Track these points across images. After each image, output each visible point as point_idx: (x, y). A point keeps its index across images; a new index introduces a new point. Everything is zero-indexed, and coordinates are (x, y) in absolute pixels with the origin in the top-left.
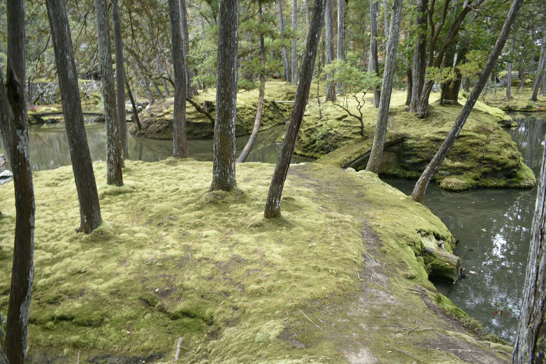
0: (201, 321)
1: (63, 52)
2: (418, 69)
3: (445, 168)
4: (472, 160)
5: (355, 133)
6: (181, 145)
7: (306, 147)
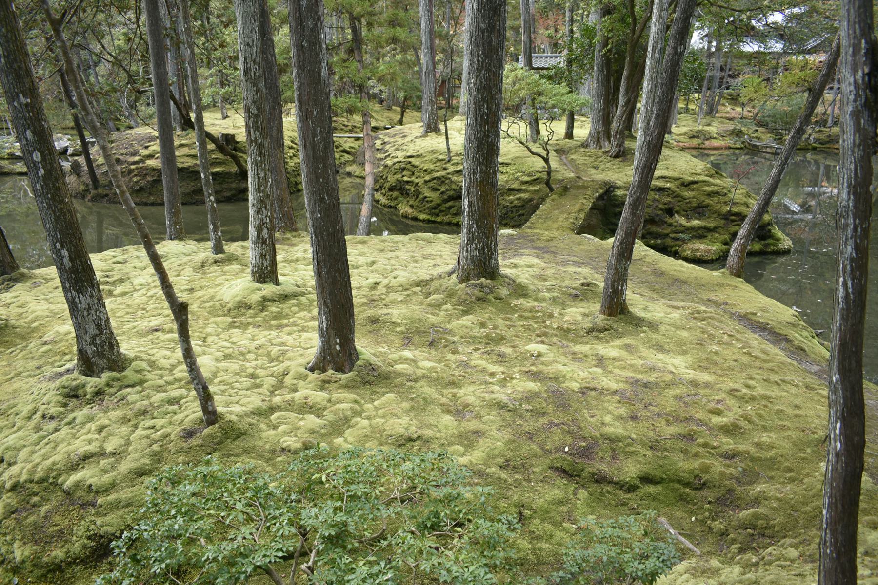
0: (677, 486)
1: (316, 25)
2: (602, 82)
3: (683, 229)
4: (715, 215)
5: (526, 182)
6: (286, 209)
7: (435, 208)
